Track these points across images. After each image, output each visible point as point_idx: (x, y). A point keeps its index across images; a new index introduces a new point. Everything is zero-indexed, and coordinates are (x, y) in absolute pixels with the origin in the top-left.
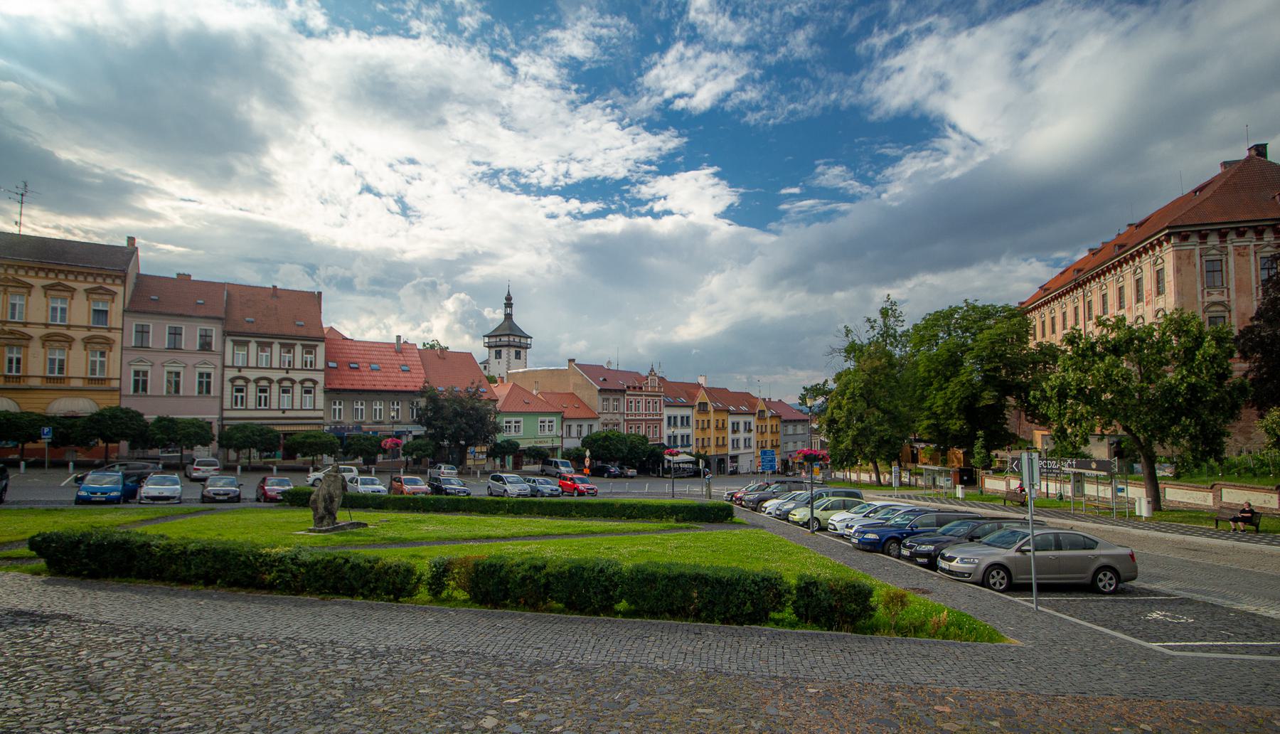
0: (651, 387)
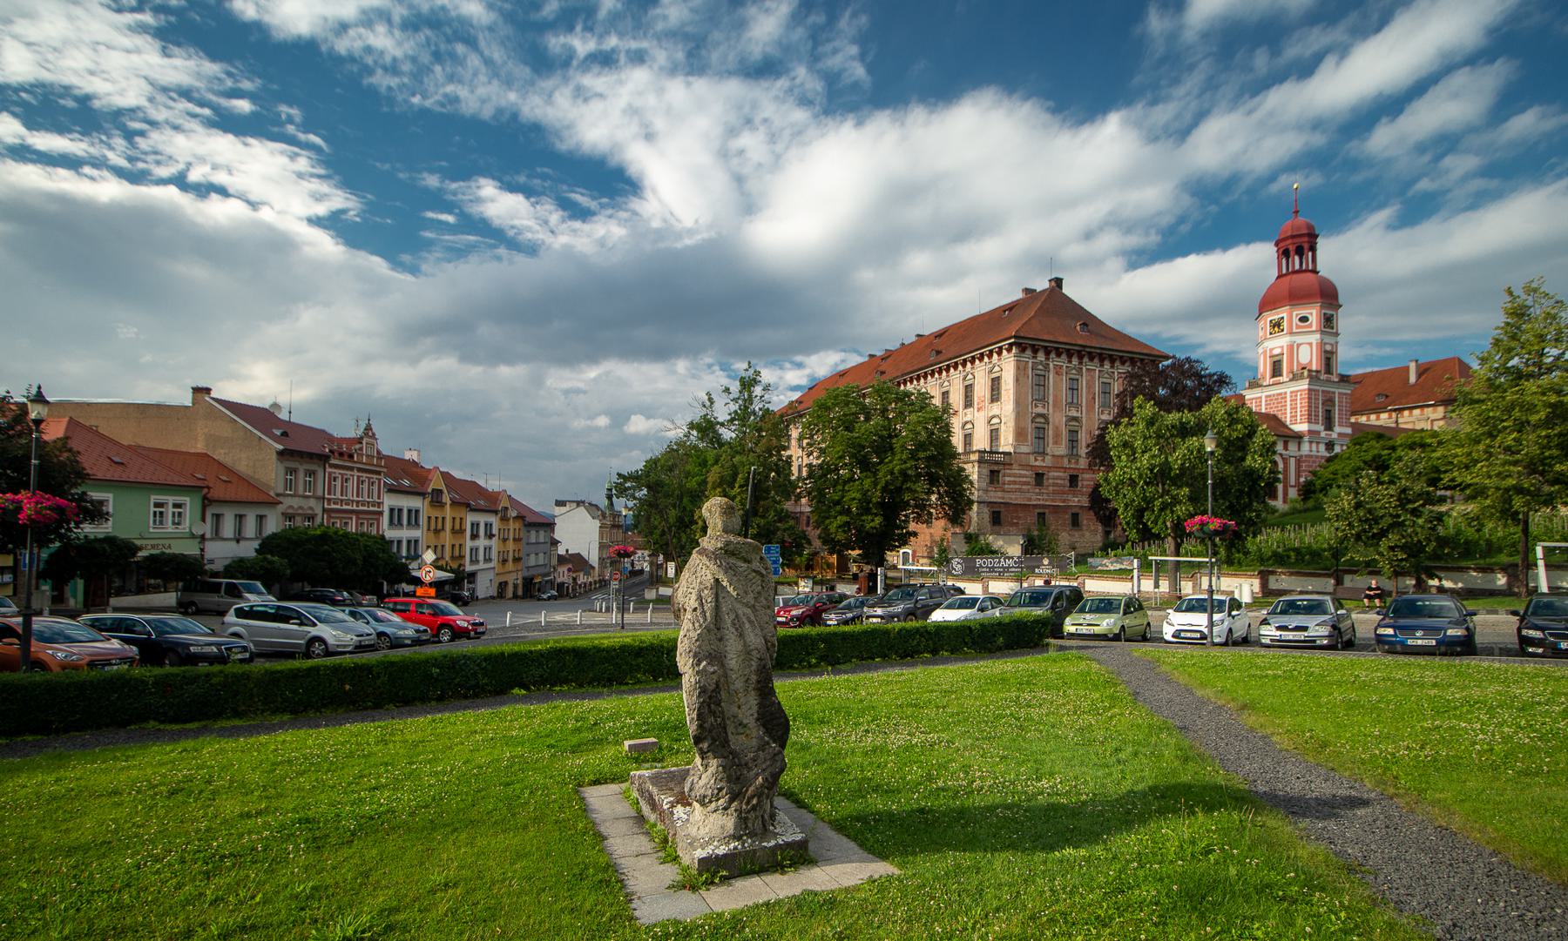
0: (367, 456)
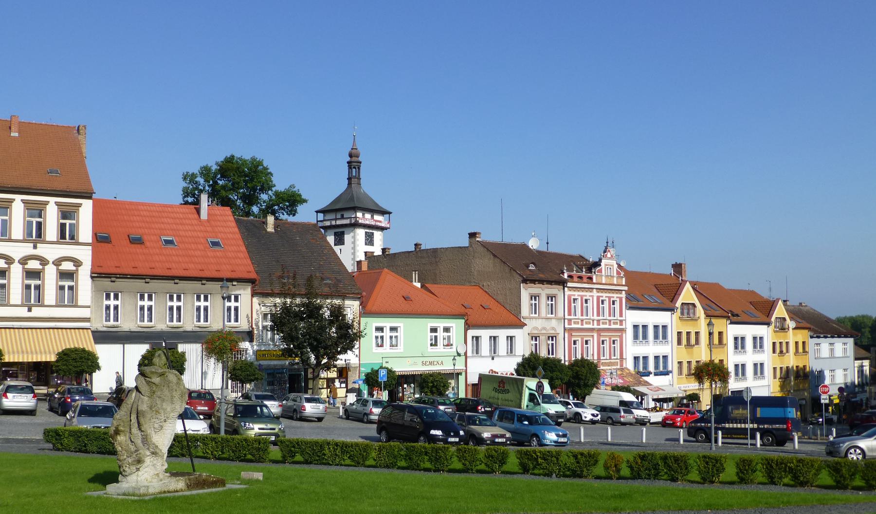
0: (607, 276)
